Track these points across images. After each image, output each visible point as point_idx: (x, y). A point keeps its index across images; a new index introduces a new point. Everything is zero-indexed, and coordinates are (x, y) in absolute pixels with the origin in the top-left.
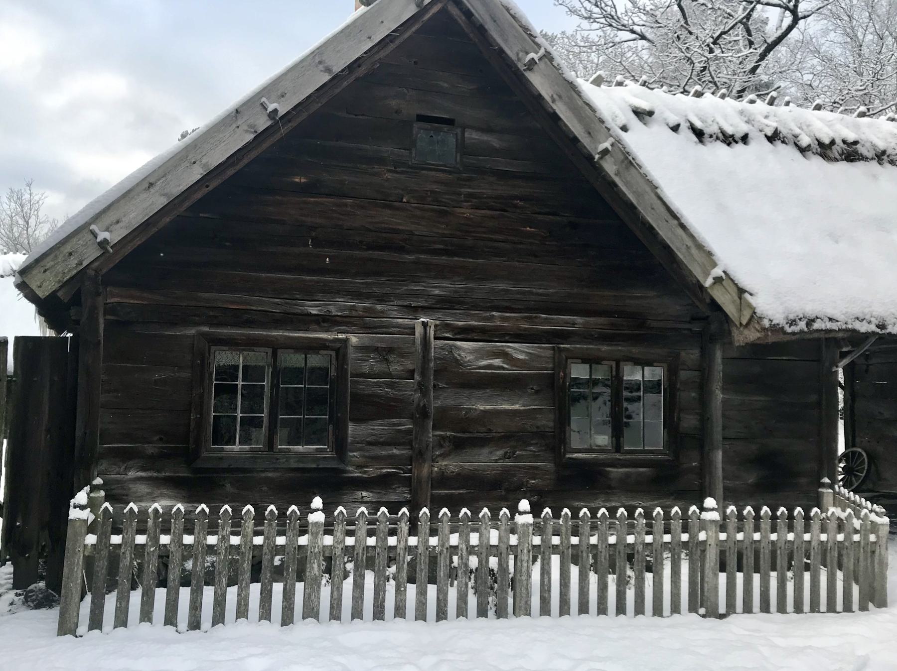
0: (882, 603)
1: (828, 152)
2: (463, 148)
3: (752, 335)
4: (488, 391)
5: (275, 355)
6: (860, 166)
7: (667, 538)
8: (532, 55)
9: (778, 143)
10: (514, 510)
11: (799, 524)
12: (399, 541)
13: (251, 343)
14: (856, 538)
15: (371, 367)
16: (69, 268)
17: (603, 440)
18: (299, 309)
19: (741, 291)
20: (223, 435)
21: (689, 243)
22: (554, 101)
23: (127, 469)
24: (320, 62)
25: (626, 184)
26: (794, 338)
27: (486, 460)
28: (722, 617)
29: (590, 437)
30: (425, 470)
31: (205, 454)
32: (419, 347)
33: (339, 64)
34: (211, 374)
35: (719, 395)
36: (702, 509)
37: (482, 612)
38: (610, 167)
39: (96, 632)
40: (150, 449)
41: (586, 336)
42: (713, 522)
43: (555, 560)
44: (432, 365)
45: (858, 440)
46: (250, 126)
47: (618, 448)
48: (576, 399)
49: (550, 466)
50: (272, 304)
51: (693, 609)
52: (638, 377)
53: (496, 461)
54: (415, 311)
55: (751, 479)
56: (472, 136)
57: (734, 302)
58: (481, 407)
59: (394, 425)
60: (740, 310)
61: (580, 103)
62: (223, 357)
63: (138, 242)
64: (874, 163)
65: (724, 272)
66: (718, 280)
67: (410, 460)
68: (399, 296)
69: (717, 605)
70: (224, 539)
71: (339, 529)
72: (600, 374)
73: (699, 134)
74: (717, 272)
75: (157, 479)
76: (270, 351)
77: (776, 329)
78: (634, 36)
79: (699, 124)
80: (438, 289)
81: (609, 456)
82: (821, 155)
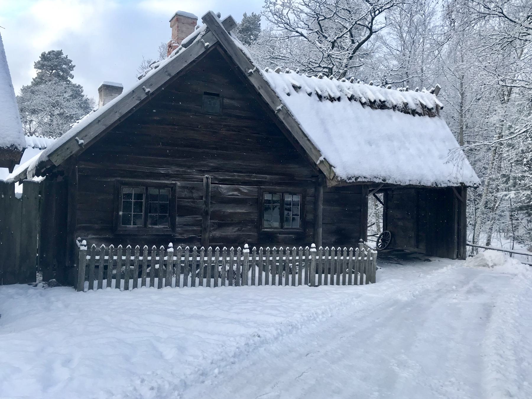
0: (374, 281)
1: (373, 105)
2: (223, 106)
3: (334, 183)
4: (232, 205)
5: (147, 189)
6: (386, 111)
7: (297, 258)
8: (251, 70)
9: (353, 101)
10: (243, 248)
11: (345, 253)
12: (201, 259)
13: (137, 185)
14: (366, 258)
15: (186, 194)
16: (67, 154)
17: (276, 224)
18: (156, 171)
19: (331, 166)
20: (126, 221)
21: (311, 147)
22: (259, 89)
23: (88, 234)
24: (166, 72)
25: (288, 123)
26: (350, 184)
27: (231, 232)
28: (317, 286)
29: (272, 223)
30: (207, 236)
31: (119, 229)
32: (205, 187)
33: (174, 73)
34: (121, 197)
35: (321, 207)
36: (310, 247)
37: (231, 284)
38: (281, 116)
39: (91, 290)
40: (97, 226)
41: (270, 183)
42: (314, 252)
43: (257, 269)
44: (210, 194)
45: (388, 227)
46: (139, 97)
47: (282, 227)
48: (267, 209)
49: (256, 234)
50: (147, 169)
51: (306, 283)
52: (290, 199)
53: (235, 232)
54: (203, 172)
55: (333, 240)
56: (226, 101)
57: (328, 170)
58: (230, 211)
59: (195, 218)
60: (330, 174)
61: (270, 90)
62: (126, 190)
63: (92, 143)
64: (392, 110)
65: (324, 158)
66: (322, 162)
67: (201, 232)
68: (197, 166)
69: (315, 282)
70: (137, 258)
71: (179, 254)
72: (276, 198)
73: (320, 97)
74: (321, 158)
75: (100, 238)
76: (145, 188)
77: (343, 181)
78: (298, 34)
79: (320, 93)
80: (213, 163)
81: (278, 230)
82: (370, 106)
